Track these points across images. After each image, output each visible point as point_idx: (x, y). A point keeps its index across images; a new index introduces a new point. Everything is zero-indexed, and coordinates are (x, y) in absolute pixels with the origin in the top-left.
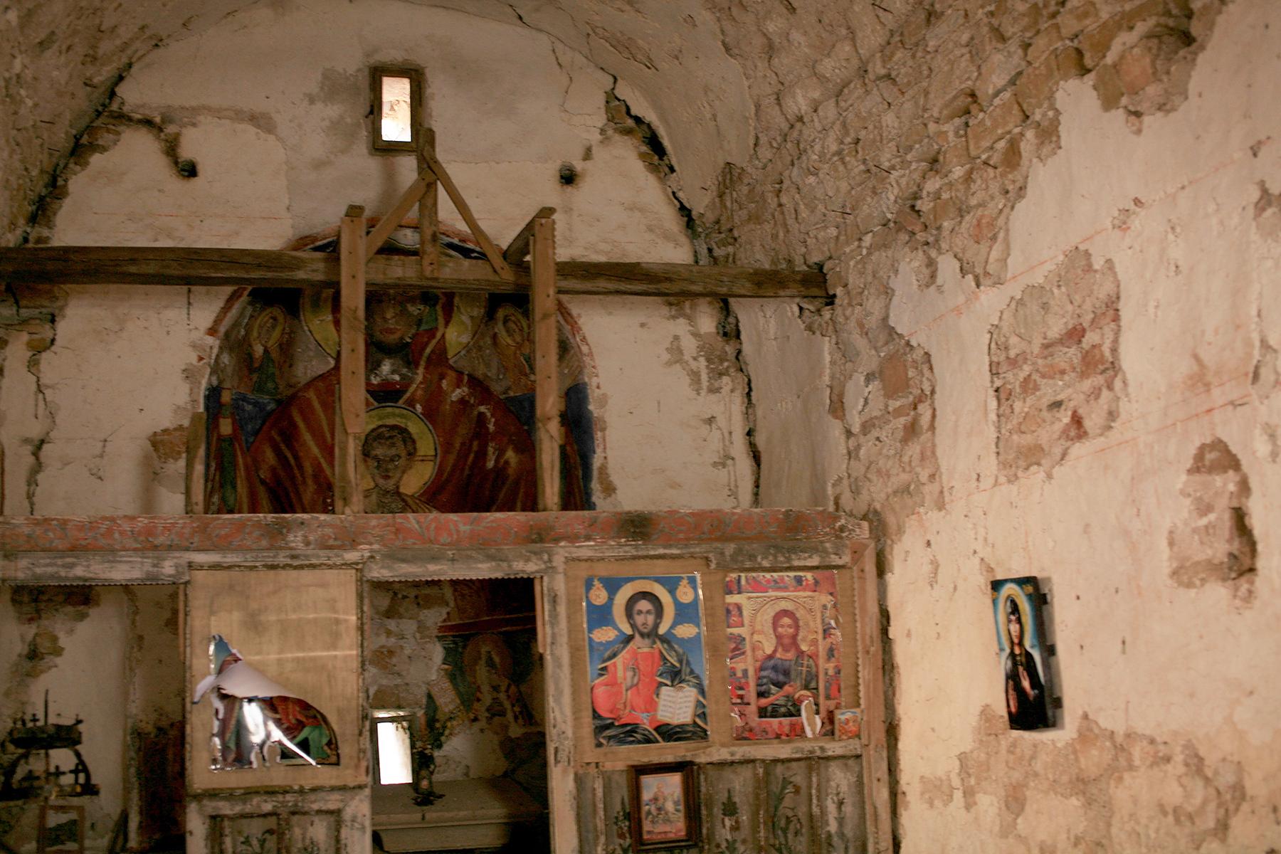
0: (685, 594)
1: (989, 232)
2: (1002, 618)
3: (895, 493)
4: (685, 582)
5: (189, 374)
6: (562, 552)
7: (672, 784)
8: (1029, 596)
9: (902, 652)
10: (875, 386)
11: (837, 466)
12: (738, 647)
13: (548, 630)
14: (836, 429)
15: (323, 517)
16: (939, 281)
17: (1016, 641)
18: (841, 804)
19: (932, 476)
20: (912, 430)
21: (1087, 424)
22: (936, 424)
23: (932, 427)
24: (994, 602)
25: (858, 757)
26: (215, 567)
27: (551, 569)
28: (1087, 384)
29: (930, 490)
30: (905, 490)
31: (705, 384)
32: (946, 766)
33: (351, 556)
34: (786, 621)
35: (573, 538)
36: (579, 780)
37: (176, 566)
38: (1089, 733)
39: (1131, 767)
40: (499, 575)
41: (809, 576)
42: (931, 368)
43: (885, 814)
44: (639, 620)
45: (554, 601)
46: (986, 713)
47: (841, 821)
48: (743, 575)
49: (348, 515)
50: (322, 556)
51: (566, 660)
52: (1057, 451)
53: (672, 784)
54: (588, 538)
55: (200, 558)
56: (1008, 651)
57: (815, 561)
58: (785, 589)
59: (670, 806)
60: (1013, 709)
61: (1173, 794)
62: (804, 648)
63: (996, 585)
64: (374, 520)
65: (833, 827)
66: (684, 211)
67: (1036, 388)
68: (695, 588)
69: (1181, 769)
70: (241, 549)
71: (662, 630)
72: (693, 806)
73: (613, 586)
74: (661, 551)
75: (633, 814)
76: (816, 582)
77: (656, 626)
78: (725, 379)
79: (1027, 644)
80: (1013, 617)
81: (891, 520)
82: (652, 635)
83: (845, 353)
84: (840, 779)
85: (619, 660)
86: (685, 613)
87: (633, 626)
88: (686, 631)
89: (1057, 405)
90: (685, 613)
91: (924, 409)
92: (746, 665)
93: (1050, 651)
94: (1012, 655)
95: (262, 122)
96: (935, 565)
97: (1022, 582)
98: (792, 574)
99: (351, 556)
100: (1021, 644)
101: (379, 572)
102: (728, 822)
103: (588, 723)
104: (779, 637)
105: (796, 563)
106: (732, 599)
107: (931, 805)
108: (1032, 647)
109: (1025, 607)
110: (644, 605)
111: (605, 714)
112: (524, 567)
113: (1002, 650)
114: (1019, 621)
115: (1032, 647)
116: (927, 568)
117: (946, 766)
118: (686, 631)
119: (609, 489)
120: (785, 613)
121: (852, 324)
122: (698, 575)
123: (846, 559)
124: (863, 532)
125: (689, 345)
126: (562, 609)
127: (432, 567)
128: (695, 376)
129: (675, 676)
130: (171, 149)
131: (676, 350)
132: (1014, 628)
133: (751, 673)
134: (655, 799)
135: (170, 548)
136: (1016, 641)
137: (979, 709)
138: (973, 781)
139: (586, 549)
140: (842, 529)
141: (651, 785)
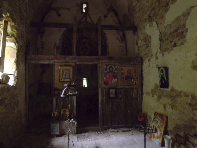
0: (116, 67)
1: (162, 17)
2: (160, 72)
3: (145, 55)
4: (116, 66)
5: (60, 40)
6: (101, 61)
7: (114, 90)
8: (165, 69)
9: (144, 75)
10: (143, 41)
11: (137, 51)
12: (123, 74)
13: (99, 71)
14: (136, 47)
15: (71, 56)
16: (153, 25)
17: (162, 75)
18: (135, 94)
19: (150, 53)
20: (147, 47)
21: (177, 44)
22: (151, 46)
23: (151, 46)
24: (159, 70)
25: (137, 88)
26: (57, 62)
27: (99, 63)
28: (178, 38)
29: (150, 55)
30: (146, 55)
31: (121, 42)
32: (149, 90)
33: (74, 61)
34: (129, 71)
35: (102, 60)
36: (102, 89)
37: (52, 62)
38: (173, 90)
39: (181, 96)
40: (93, 64)
41: (132, 65)
42: (151, 38)
43: (141, 96)
44: (110, 70)
45: (100, 67)
46: (156, 85)
47: (135, 96)
48: (124, 65)
49: (74, 56)
50: (70, 61)
51: (101, 75)
52: (171, 49)
53: (114, 90)
54: (104, 60)
55: (55, 61)
56: (160, 77)
57: (133, 63)
58: (129, 67)
59: (113, 93)
60: (161, 85)
61: (189, 101)
62: (131, 74)
63: (159, 68)
64: (77, 57)
65: (134, 97)
66: (119, 21)
67: (168, 40)
68: (117, 66)
69: (191, 98)
70: (60, 60)
71: (113, 71)
72: (116, 93)
73: (107, 65)
74: (114, 61)
75: (109, 94)
76: (133, 66)
77: (112, 71)
78: (123, 41)
79: (164, 76)
80: (162, 72)
81: (144, 59)
82: (112, 72)
83: (138, 38)
84: (135, 91)
85: (108, 75)
86: (116, 69)
87: (109, 70)
88: (116, 72)
89: (171, 42)
90: (116, 69)
91: (149, 44)
92: (124, 76)
93: (167, 77)
94: (161, 77)
95: (68, 9)
96: (149, 65)
97: (164, 67)
98: (130, 65)
99: (74, 61)
100: (163, 76)
101: (78, 63)
102: (121, 95)
103: (103, 82)
104: (128, 73)
105: (131, 63)
106: (122, 68)
107: (147, 95)
108: (165, 77)
109: (164, 71)
110: (111, 68)
111: (105, 81)
112: (97, 63)
113: (159, 76)
114: (163, 73)
115: (165, 77)
116: (148, 65)
117: (149, 90)
118: (116, 72)
119: (109, 54)
120: (129, 70)
121: (140, 33)
122: (118, 65)
123: (137, 63)
124: (140, 60)
125: (119, 37)
126: (101, 68)
127: (84, 63)
128: (120, 42)
129: (115, 77)
130: (57, 13)
131: (117, 38)
132: (162, 74)
133: (124, 77)
134: (111, 92)
135: (51, 60)
136: (162, 75)
137: (155, 84)
138: (153, 93)
139: (104, 61)
140: (137, 59)
141: (111, 91)
